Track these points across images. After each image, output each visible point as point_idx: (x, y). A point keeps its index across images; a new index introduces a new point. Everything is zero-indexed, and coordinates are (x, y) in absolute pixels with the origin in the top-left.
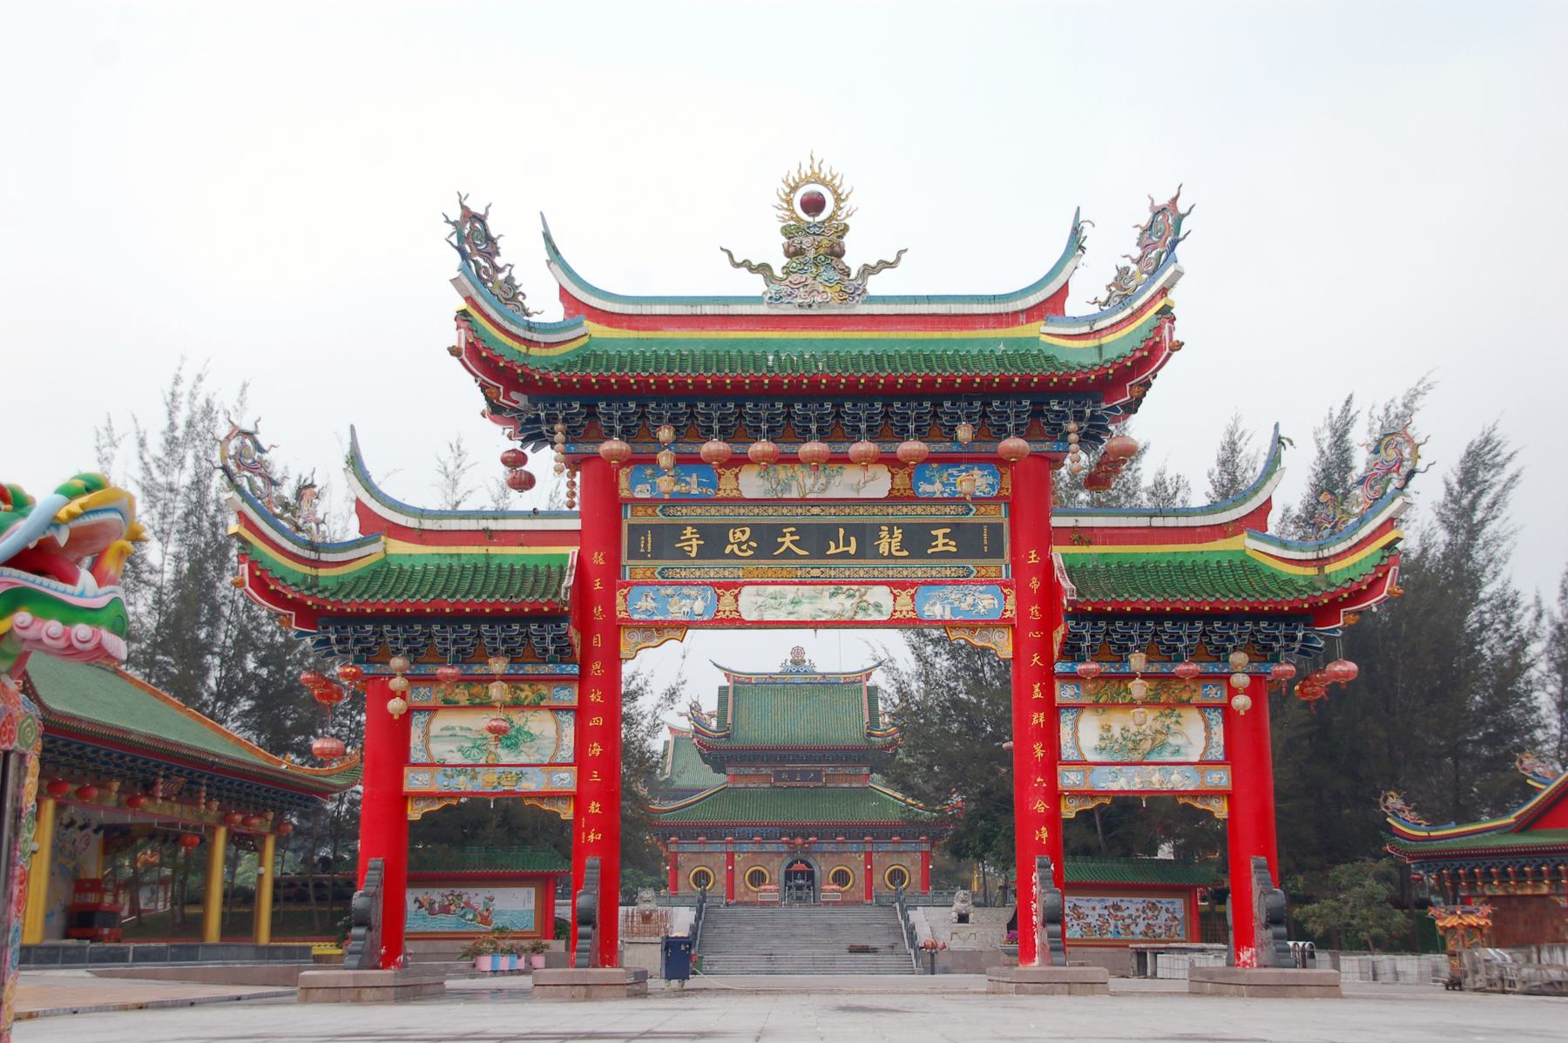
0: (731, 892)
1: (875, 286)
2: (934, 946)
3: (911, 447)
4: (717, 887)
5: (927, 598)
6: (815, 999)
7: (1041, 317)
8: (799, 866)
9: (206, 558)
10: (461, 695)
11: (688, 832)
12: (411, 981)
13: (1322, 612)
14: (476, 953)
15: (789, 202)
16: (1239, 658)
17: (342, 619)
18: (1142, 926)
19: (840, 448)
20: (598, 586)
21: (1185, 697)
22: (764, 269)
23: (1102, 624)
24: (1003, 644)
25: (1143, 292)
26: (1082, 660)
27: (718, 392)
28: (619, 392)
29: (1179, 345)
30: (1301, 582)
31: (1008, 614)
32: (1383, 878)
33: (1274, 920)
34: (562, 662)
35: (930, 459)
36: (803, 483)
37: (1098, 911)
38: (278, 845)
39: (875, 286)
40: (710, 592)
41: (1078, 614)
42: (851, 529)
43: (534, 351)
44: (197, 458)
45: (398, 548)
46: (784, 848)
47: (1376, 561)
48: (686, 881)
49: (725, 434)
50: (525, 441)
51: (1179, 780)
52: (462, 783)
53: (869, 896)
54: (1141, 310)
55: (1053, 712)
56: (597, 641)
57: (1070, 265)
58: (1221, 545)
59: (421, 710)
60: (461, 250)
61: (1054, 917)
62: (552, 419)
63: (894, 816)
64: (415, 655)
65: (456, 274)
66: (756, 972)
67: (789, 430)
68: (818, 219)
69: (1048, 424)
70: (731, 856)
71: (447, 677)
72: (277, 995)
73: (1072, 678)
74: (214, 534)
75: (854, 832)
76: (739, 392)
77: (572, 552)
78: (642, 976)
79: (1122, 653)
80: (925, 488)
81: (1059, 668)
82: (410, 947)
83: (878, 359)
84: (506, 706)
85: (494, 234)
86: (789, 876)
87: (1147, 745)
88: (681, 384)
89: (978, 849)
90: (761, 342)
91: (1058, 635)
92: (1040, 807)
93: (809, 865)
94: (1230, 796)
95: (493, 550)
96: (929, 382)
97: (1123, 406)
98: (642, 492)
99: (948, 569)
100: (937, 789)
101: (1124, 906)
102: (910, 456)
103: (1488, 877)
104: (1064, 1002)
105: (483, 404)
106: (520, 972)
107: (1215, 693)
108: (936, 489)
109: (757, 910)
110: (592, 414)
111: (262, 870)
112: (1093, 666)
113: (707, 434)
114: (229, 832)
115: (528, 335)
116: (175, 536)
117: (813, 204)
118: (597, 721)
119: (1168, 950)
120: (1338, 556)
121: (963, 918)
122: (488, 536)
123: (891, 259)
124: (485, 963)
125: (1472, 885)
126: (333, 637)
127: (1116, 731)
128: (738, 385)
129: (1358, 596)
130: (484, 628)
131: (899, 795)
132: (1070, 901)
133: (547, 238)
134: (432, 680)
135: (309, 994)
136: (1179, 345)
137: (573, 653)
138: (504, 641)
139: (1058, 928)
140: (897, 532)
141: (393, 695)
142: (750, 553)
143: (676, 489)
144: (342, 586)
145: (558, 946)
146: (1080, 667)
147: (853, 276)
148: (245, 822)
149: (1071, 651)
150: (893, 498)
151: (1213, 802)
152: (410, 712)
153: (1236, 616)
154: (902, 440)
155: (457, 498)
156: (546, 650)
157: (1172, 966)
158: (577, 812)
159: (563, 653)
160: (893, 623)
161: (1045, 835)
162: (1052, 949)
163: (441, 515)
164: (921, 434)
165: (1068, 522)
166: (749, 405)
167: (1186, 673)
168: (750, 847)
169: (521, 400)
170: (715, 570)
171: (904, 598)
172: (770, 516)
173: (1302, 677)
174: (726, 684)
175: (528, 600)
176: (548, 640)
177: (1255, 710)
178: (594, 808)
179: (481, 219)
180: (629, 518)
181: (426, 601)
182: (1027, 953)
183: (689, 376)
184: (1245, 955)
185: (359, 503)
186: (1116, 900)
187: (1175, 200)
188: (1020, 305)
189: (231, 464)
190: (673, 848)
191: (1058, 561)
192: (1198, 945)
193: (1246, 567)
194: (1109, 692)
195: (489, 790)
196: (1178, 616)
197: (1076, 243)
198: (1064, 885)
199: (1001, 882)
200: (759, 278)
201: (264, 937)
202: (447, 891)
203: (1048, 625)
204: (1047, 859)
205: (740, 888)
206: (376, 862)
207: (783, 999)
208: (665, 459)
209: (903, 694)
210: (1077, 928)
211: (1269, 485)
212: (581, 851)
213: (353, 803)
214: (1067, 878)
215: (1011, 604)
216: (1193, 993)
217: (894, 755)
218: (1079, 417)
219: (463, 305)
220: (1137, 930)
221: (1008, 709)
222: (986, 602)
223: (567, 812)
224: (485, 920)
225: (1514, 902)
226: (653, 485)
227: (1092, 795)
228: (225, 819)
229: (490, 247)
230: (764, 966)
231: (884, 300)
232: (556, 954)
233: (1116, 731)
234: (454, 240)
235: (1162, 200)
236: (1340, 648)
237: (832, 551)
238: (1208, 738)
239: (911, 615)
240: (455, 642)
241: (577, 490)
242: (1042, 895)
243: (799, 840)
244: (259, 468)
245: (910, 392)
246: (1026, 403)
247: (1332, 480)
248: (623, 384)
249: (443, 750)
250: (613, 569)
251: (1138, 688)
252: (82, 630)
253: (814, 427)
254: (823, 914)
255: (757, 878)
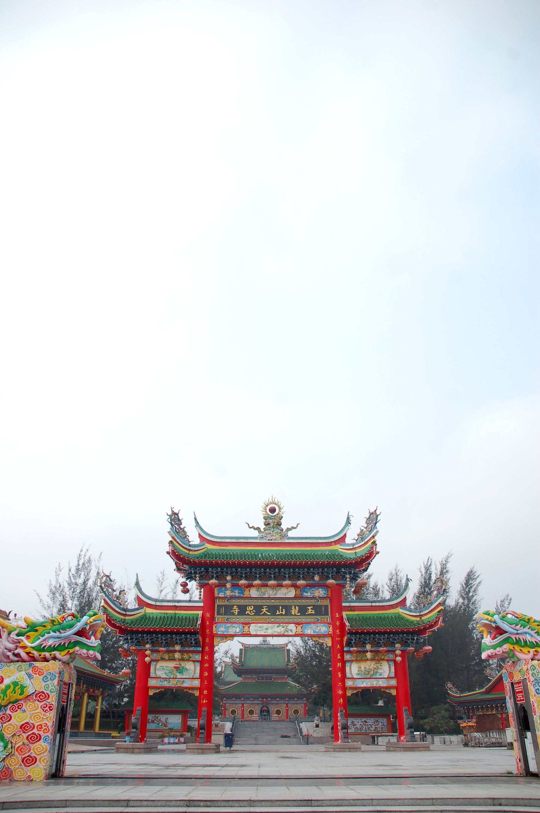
0: (243, 718)
1: (291, 534)
2: (308, 735)
3: (301, 582)
4: (238, 714)
5: (306, 628)
6: (273, 754)
7: (339, 543)
8: (265, 708)
9: (85, 606)
10: (166, 656)
11: (230, 697)
12: (149, 746)
13: (421, 631)
14: (163, 737)
15: (266, 509)
16: (398, 645)
17: (132, 632)
18: (374, 728)
19: (280, 582)
20: (208, 624)
21: (383, 657)
22: (258, 529)
23: (358, 636)
24: (328, 642)
25: (368, 537)
26: (352, 647)
27: (244, 566)
28: (216, 565)
29: (378, 553)
30: (415, 622)
31: (330, 633)
32: (446, 710)
33: (410, 727)
34: (197, 646)
35: (307, 585)
36: (269, 593)
37: (360, 723)
38: (103, 700)
39: (291, 534)
40: (241, 626)
41: (351, 633)
42: (284, 607)
43: (191, 553)
44: (85, 575)
45: (149, 610)
46: (260, 702)
47: (436, 616)
48: (228, 713)
49: (246, 578)
50: (187, 579)
51: (382, 683)
52: (166, 684)
53: (287, 718)
54: (367, 542)
55: (344, 662)
56: (207, 640)
57: (347, 528)
58: (392, 611)
59: (154, 660)
60: (171, 523)
61: (345, 727)
62: (195, 573)
63: (295, 691)
64: (153, 644)
65: (170, 530)
66: (251, 744)
67: (265, 577)
68: (274, 514)
69: (341, 575)
70: (243, 704)
71: (162, 651)
72: (106, 750)
73: (349, 652)
74: (89, 598)
75: (282, 697)
76: (251, 566)
77: (200, 613)
78: (218, 746)
79: (364, 644)
80: (305, 594)
81: (345, 649)
82: (148, 734)
83: (291, 556)
84: (179, 660)
85: (180, 518)
86: (261, 711)
87: (372, 673)
88: (234, 563)
89: (322, 703)
90: (257, 550)
91: (345, 639)
92: (340, 692)
93: (268, 708)
94: (397, 688)
95: (177, 612)
96: (306, 563)
97: (363, 570)
98: (221, 595)
99: (312, 619)
100: (309, 683)
101: (368, 721)
102: (301, 585)
103: (478, 709)
104: (347, 754)
105: (175, 567)
106: (176, 743)
107: (391, 656)
108: (308, 595)
109: (251, 723)
110: (207, 571)
111: (97, 707)
112: (355, 649)
113: (241, 578)
114: (88, 695)
115: (189, 548)
116: (76, 599)
117: (273, 510)
118: (207, 665)
119: (381, 736)
120: (426, 614)
121: (317, 726)
122: (175, 608)
123: (295, 526)
124: (166, 740)
125: (473, 712)
126: (129, 638)
127: (363, 669)
128: (250, 563)
129: (431, 626)
130: (174, 636)
131: (297, 685)
132: (350, 720)
133: (196, 519)
134: (158, 651)
135: (119, 750)
136: (378, 553)
137: (200, 644)
138: (180, 640)
139: (346, 731)
140: (297, 607)
141: (146, 656)
142: (253, 614)
143: (232, 594)
144: (132, 622)
145: (188, 734)
146: (352, 649)
147: (284, 531)
148: (93, 691)
149: (349, 644)
150: (296, 597)
151: (392, 690)
152: (152, 660)
153: (397, 633)
154: (299, 580)
155: (162, 589)
156: (192, 643)
157: (382, 741)
158: (200, 694)
159: (197, 644)
160: (296, 635)
161: (342, 701)
162: (344, 737)
163: (162, 601)
164: (304, 579)
165: (348, 604)
166: (254, 569)
167: (383, 650)
168: (249, 702)
169: (187, 567)
170: (243, 619)
171: (299, 627)
172: (259, 603)
173: (416, 650)
174: (242, 648)
175: (187, 628)
176: (193, 640)
177: (403, 661)
178: (205, 692)
179: (177, 514)
180: (217, 603)
181: (157, 627)
182: (336, 739)
183: (236, 561)
184: (402, 738)
185: (138, 597)
186: (365, 719)
187: (376, 510)
188: (333, 540)
189: (103, 585)
190: (224, 702)
191: (345, 616)
192: (391, 734)
193: (399, 618)
194: (360, 657)
195: (173, 686)
196: (380, 633)
197: (348, 522)
198: (347, 715)
199: (329, 713)
200: (257, 531)
201: (97, 730)
202: (153, 716)
203: (342, 636)
204: (342, 709)
205: (246, 716)
206: (139, 708)
207: (263, 754)
208: (228, 585)
209: (298, 652)
210: (353, 729)
211: (405, 593)
212: (201, 706)
213: (125, 686)
214: (349, 712)
215: (331, 630)
216: (387, 751)
217: (295, 671)
218: (350, 573)
219: (171, 539)
220: (372, 729)
221: (331, 657)
222: (323, 629)
223: (197, 693)
224: (166, 726)
225: (486, 716)
226: (225, 593)
227: (356, 688)
228: (88, 690)
229: (179, 522)
230: (254, 742)
231: (293, 538)
232: (187, 737)
233: (363, 669)
234: (169, 520)
235: (372, 510)
236: (427, 642)
237: (278, 613)
238: (390, 670)
239: (301, 633)
240: (165, 640)
241: (202, 593)
242: (341, 720)
243: (265, 700)
244: (110, 586)
245: (301, 566)
246: (335, 569)
247: (426, 585)
248: (217, 563)
249: (160, 673)
250: (212, 618)
251: (369, 655)
252: (91, 652)
253: (272, 576)
254: (273, 725)
255: (251, 712)
